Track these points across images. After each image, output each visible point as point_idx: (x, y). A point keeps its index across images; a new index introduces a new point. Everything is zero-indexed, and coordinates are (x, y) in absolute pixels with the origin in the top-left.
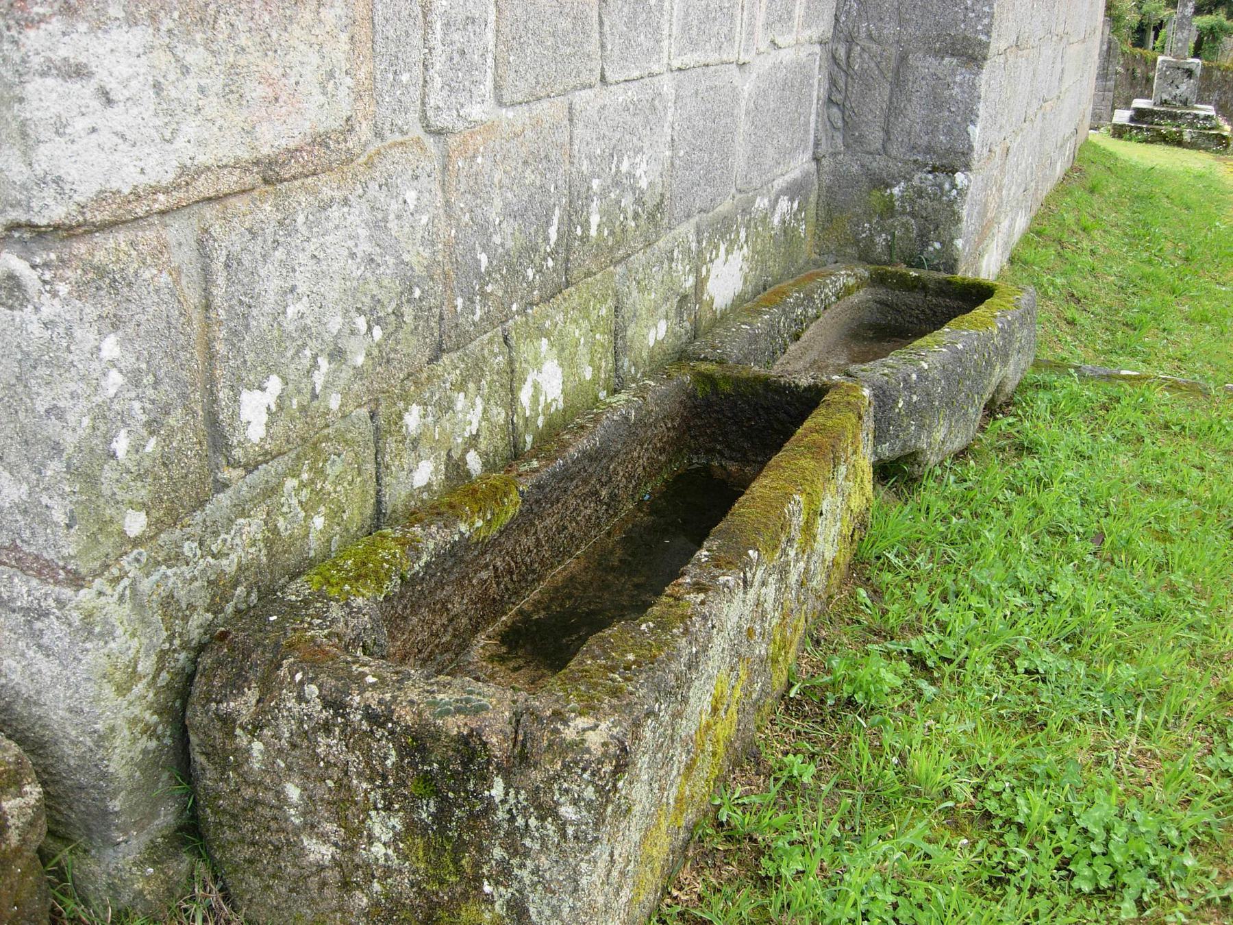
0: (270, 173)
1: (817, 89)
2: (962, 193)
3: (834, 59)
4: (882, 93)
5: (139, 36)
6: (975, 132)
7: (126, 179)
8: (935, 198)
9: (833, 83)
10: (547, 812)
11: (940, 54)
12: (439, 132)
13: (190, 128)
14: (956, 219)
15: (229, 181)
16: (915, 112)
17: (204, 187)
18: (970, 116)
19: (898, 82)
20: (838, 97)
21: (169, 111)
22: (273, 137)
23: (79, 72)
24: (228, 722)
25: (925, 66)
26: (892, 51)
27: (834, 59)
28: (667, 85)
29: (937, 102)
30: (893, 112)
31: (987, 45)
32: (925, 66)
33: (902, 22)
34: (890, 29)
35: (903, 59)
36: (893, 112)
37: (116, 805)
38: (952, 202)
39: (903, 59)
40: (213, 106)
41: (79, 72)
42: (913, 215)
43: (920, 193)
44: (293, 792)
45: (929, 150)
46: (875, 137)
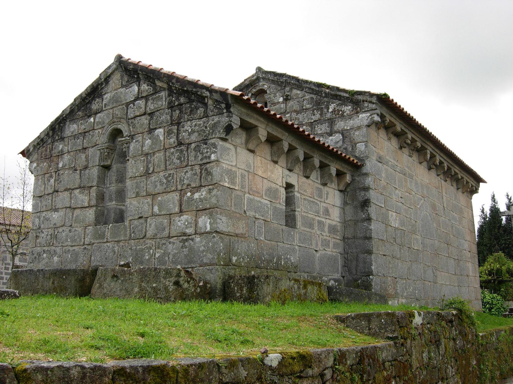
0: (237, 235)
1: (340, 262)
2: (372, 280)
3: (345, 258)
4: (354, 263)
5: (225, 218)
6: (373, 267)
7: (224, 230)
8: (367, 282)
9: (345, 262)
10: (260, 281)
11: (364, 253)
12: (257, 239)
13: (229, 228)
14: (371, 285)
15: (233, 234)
16: (361, 265)
17: (230, 234)
18: (371, 265)
19: (357, 260)
20: (346, 265)
21: (228, 225)
22: (237, 232)
23: (221, 219)
24: (229, 283)
25: (362, 256)
26: (356, 254)
27: (345, 258)
28: (297, 247)
29: (365, 263)
30: (357, 266)
31: (372, 250)
32: (362, 256)
33: (357, 249)
34: (354, 251)
35: (357, 255)
36: (357, 266)
37: (217, 291)
38: (370, 282)
39: (357, 255)
40: (232, 227)
41: (221, 219)
42: (363, 286)
43: (364, 281)
44: (236, 288)
45: (364, 273)
46: (354, 272)
